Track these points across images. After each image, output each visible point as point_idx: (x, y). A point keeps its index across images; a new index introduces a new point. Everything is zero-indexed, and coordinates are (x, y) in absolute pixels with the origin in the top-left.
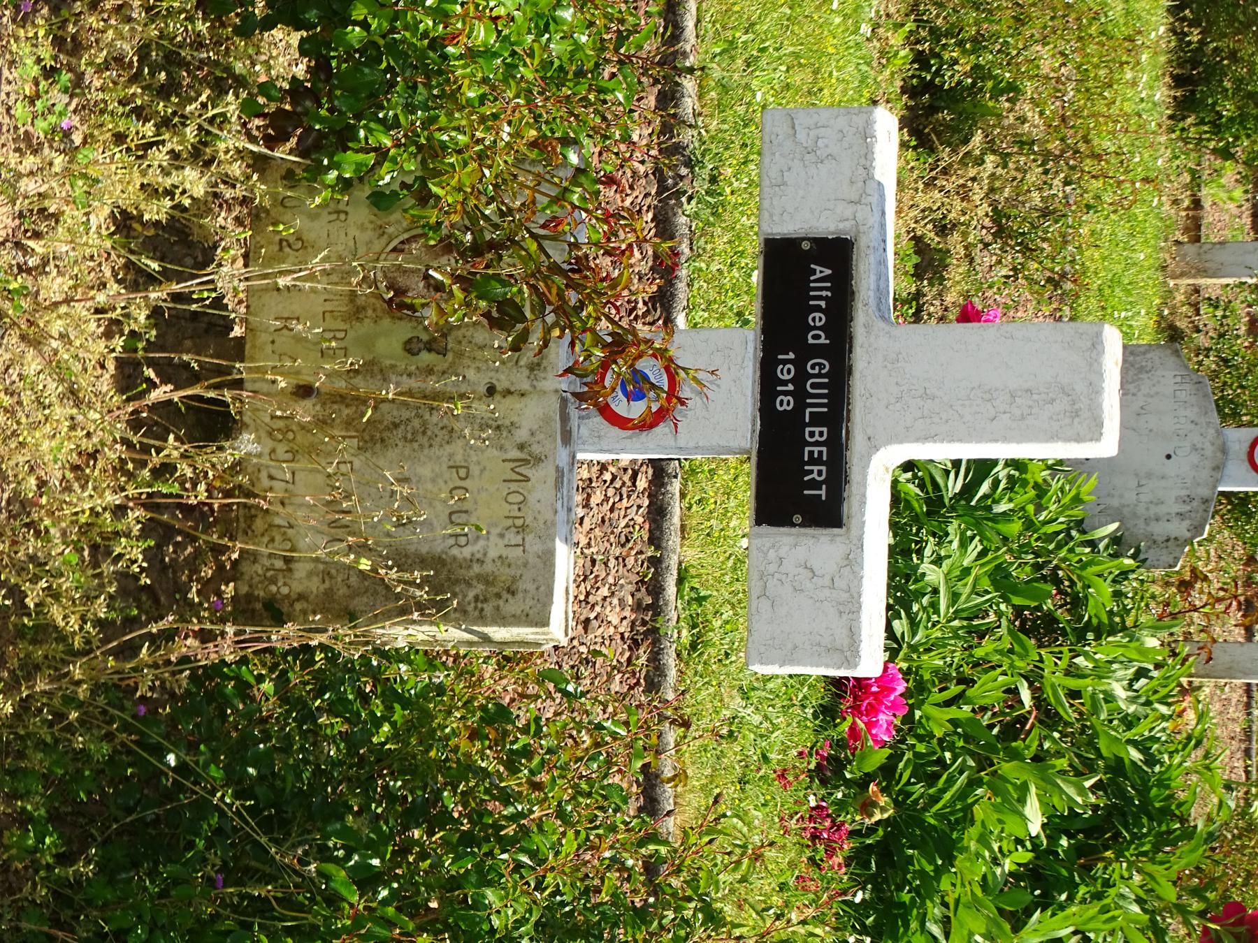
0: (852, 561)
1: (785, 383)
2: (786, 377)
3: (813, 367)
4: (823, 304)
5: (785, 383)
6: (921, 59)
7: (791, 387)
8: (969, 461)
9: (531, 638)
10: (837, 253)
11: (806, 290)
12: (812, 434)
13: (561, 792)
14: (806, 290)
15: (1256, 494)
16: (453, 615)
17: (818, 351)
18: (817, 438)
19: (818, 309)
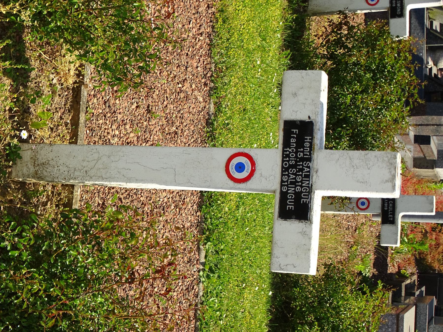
0: (308, 236)
3: (289, 196)
4: (295, 136)
6: (72, 193)
8: (321, 210)
14: (297, 134)
16: (123, 191)
19: (294, 137)
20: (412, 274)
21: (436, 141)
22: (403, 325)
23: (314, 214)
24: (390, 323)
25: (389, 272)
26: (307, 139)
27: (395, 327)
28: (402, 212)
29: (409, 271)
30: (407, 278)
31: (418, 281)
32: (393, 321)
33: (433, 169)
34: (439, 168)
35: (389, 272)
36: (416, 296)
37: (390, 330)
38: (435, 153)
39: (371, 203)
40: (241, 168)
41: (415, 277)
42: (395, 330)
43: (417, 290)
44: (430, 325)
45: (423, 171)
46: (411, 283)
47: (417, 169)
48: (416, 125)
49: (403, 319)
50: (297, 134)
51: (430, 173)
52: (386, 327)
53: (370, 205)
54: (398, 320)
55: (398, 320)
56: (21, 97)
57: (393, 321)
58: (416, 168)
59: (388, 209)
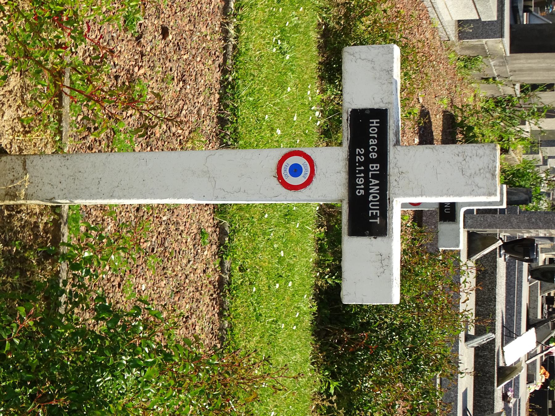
1: (360, 185)
2: (360, 183)
3: (377, 167)
4: (376, 136)
5: (360, 185)
7: (362, 187)
8: (402, 208)
9: (500, 315)
10: (381, 114)
11: (367, 134)
12: (372, 167)
18: (375, 168)
26: (373, 123)
40: (294, 171)
43: (498, 386)
50: (367, 134)
56: (61, 296)
59: (367, 194)
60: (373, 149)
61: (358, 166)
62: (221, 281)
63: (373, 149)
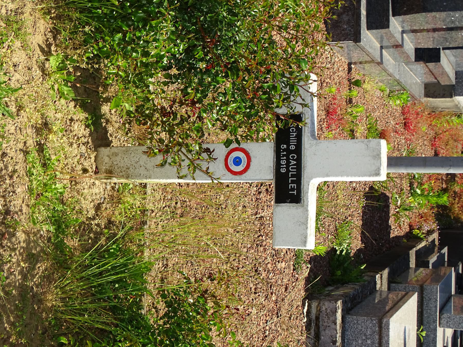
1: (283, 165)
2: (283, 163)
5: (283, 165)
7: (285, 166)
13: (170, 93)
15: (462, 176)
17: (293, 152)
20: (430, 232)
21: (452, 59)
22: (388, 336)
23: (308, 159)
24: (369, 332)
25: (392, 236)
27: (377, 337)
28: (319, 177)
29: (426, 228)
30: (421, 240)
31: (439, 240)
32: (374, 328)
33: (451, 97)
34: (460, 95)
35: (392, 236)
36: (431, 267)
37: (369, 342)
38: (452, 75)
39: (253, 159)
41: (435, 236)
42: (377, 342)
44: (443, 314)
45: (439, 101)
46: (426, 245)
47: (431, 99)
48: (414, 31)
49: (389, 326)
51: (449, 104)
52: (364, 338)
53: (252, 164)
54: (380, 327)
55: (380, 327)
57: (374, 328)
58: (429, 97)
59: (288, 171)
60: (293, 130)
61: (282, 152)
62: (42, 151)
63: (293, 130)
